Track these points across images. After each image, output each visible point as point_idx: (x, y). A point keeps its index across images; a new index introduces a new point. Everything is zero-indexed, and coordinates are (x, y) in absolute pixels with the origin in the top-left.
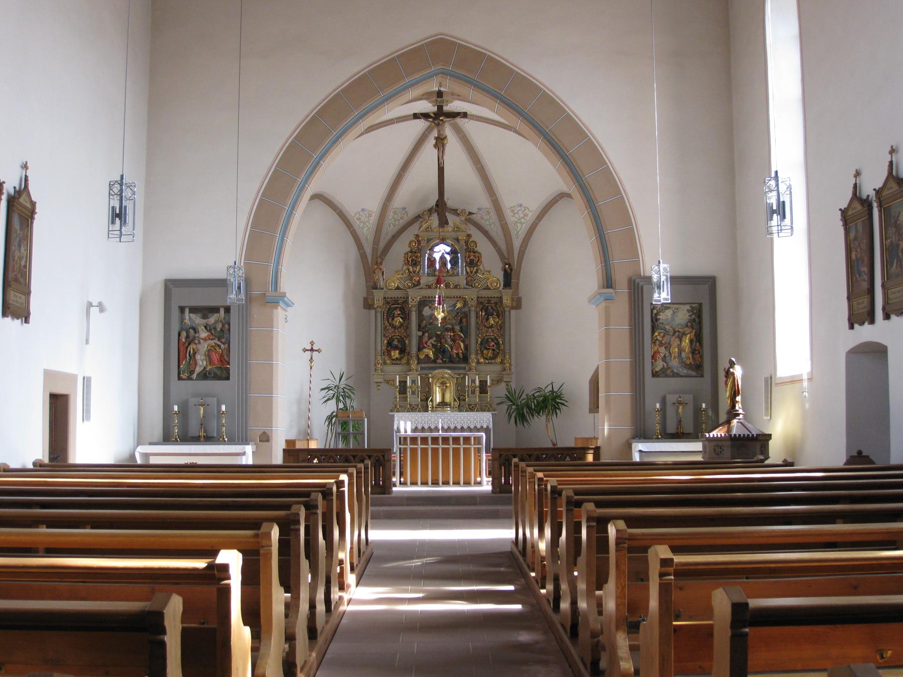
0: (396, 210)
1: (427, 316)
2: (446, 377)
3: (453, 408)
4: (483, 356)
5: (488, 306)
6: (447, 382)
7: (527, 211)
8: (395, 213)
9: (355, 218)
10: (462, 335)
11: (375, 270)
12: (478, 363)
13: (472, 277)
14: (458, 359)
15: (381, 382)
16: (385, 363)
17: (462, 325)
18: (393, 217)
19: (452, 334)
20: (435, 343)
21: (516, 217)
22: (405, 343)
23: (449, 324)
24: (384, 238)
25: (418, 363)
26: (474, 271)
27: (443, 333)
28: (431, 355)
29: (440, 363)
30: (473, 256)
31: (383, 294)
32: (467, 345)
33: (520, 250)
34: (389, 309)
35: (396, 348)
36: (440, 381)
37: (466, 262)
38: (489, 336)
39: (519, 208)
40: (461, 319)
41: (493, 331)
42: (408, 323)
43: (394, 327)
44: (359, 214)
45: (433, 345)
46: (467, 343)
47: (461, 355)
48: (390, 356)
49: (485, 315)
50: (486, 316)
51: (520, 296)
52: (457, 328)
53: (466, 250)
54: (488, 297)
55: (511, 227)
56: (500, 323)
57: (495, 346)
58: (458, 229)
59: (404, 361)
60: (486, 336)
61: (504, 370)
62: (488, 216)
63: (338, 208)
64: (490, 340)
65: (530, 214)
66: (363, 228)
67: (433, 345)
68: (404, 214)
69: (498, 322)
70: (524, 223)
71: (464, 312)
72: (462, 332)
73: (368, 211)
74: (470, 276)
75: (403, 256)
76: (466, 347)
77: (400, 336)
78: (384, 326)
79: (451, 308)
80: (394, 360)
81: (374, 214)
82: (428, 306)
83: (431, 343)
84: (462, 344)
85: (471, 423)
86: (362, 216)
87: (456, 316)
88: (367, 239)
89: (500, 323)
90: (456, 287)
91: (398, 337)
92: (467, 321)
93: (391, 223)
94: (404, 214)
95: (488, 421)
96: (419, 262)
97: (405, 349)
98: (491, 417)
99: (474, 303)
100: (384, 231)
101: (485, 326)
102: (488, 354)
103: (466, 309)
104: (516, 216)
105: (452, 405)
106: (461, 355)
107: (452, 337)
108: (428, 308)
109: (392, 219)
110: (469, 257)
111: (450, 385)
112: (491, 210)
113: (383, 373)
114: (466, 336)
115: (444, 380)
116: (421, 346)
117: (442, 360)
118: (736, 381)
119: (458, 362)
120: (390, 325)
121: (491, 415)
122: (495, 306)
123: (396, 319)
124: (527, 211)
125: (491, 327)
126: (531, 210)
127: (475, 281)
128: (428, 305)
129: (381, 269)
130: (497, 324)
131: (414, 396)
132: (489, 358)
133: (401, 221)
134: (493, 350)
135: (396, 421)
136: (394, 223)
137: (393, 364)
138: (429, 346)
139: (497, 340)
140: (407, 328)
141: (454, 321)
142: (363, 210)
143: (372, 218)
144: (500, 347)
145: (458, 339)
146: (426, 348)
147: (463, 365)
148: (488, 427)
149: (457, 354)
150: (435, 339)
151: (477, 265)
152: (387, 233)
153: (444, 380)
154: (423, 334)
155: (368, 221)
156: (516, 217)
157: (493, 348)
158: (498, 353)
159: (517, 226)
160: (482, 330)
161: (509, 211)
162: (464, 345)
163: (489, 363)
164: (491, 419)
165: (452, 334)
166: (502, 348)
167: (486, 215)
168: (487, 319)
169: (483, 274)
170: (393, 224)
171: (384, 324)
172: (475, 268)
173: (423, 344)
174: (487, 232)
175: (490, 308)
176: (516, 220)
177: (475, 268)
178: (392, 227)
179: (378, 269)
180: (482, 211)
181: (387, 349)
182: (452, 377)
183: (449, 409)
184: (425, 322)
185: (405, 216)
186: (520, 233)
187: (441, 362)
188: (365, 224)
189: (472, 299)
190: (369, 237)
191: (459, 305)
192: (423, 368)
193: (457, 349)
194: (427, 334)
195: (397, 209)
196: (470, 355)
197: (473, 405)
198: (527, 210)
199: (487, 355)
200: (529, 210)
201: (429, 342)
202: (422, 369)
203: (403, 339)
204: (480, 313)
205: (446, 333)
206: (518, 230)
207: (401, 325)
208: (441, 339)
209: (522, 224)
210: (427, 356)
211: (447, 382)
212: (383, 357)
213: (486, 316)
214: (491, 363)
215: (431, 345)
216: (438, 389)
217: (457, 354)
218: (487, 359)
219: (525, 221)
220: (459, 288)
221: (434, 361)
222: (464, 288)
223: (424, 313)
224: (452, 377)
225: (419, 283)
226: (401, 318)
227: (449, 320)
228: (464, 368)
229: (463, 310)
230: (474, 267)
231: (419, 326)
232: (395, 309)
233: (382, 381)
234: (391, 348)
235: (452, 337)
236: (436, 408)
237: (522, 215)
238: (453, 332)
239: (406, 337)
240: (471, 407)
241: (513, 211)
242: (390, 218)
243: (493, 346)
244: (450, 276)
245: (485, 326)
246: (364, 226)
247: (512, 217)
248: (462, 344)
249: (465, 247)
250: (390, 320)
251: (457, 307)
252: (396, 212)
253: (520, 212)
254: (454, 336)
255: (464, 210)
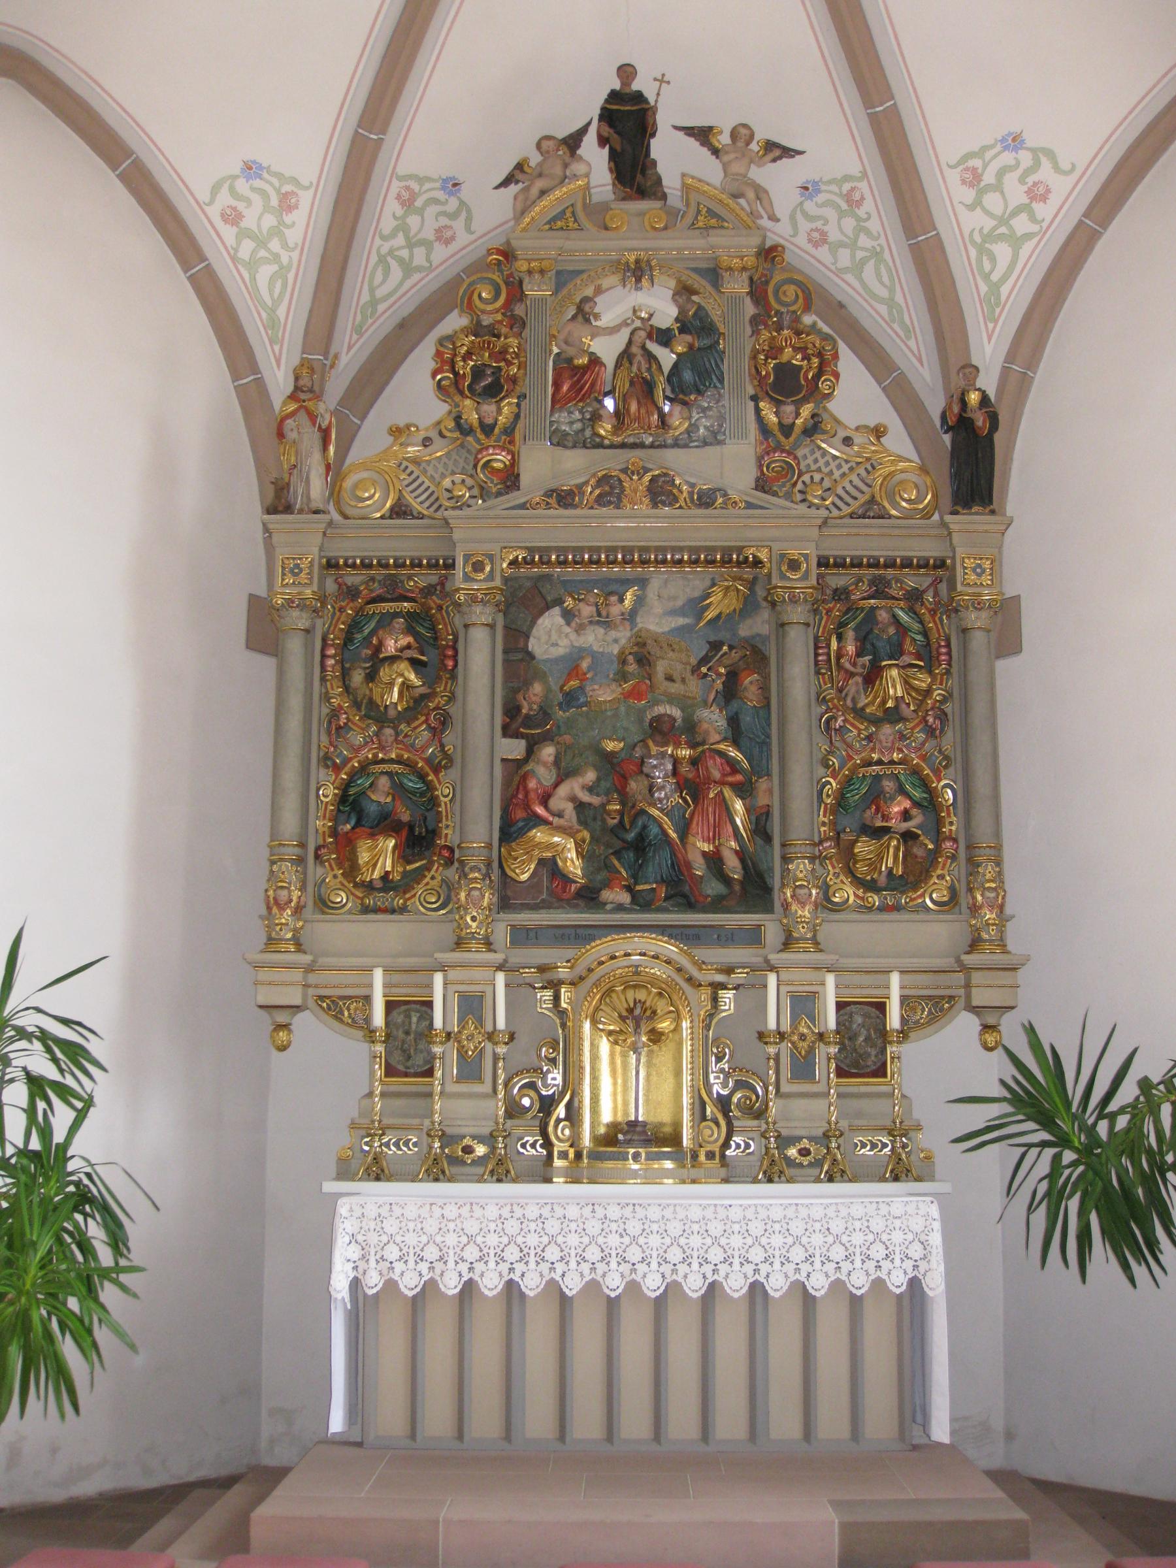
0: (415, 186)
1: (557, 661)
2: (654, 980)
3: (695, 1156)
4: (851, 873)
5: (873, 609)
6: (662, 1006)
7: (1045, 173)
8: (408, 202)
9: (214, 212)
10: (740, 756)
11: (283, 420)
12: (826, 904)
13: (789, 453)
14: (713, 888)
15: (296, 1009)
16: (324, 904)
17: (735, 705)
18: (403, 228)
19: (685, 753)
20: (596, 800)
21: (987, 212)
22: (434, 802)
23: (670, 703)
24: (359, 330)
25: (505, 904)
26: (799, 422)
27: (638, 753)
28: (573, 864)
29: (620, 908)
30: (796, 349)
31: (319, 538)
32: (767, 813)
33: (1005, 372)
34: (354, 626)
35: (385, 823)
36: (620, 1002)
37: (761, 380)
38: (880, 762)
39: (1008, 158)
40: (732, 678)
41: (902, 737)
42: (452, 698)
43: (375, 713)
44: (232, 190)
45: (580, 806)
46: (762, 800)
47: (732, 863)
48: (351, 869)
49: (859, 654)
50: (867, 659)
51: (1010, 592)
52: (713, 720)
53: (755, 321)
54: (875, 565)
55: (960, 260)
56: (937, 694)
57: (918, 818)
58: (713, 222)
59: (423, 895)
60: (868, 763)
61: (975, 944)
62: (849, 224)
63: (128, 152)
64: (888, 785)
65: (1060, 186)
66: (253, 265)
67: (580, 806)
68: (454, 216)
69: (928, 692)
70: (1028, 236)
71: (745, 640)
72: (736, 743)
73: (279, 176)
74: (779, 448)
75: (433, 351)
76: (761, 826)
77: (409, 764)
78: (325, 710)
79: (681, 621)
80: (369, 887)
81: (305, 198)
82: (556, 610)
83: (573, 799)
84: (739, 806)
85: (809, 1259)
86: (249, 202)
87: (704, 661)
88: (272, 324)
89: (937, 694)
90: (705, 500)
91: (396, 767)
92: (764, 688)
93: (391, 252)
94: (454, 216)
95: (916, 1251)
96: (514, 380)
97: (434, 833)
98: (937, 1225)
99: (801, 583)
100: (356, 293)
101: (859, 713)
102: (880, 858)
103: (758, 625)
104: (992, 201)
105: (686, 1142)
106: (732, 863)
107: (685, 769)
108: (561, 621)
109: (393, 235)
110: (774, 351)
111: (677, 1029)
112: (863, 185)
113: (307, 959)
114: (760, 769)
115: (641, 995)
116: (520, 814)
117: (629, 889)
118: (992, 1123)
119: (718, 905)
120: (357, 704)
121: (934, 1210)
122: (912, 611)
123: (384, 673)
124: (1045, 173)
125: (893, 715)
126: (1066, 166)
127: (806, 478)
128: (559, 602)
129: (313, 417)
130: (920, 704)
131: (477, 1088)
132: (883, 880)
133: (440, 252)
134: (908, 837)
135: (341, 1241)
136: (405, 253)
137: (366, 910)
138: (560, 815)
139: (924, 784)
140: (445, 721)
141: (694, 687)
142: (251, 169)
143: (298, 217)
144: (939, 822)
145: (716, 775)
146: (546, 822)
147: (748, 919)
148: (915, 1284)
149: (714, 860)
150: (590, 776)
151: (813, 392)
152: (374, 303)
153: (641, 995)
154: (530, 752)
155: (276, 232)
156: (987, 212)
157: (905, 826)
158: (937, 851)
159: (993, 259)
160: (841, 731)
161: (954, 177)
162: (748, 810)
163: (884, 908)
164: (936, 1239)
165: (685, 753)
166: (953, 825)
167: (842, 214)
168: (872, 676)
169: (848, 441)
170: (400, 261)
171: (326, 697)
172: (806, 410)
173: (527, 806)
174: (841, 306)
175: (883, 616)
176: (989, 224)
177: (806, 410)
178: (396, 273)
179: (303, 417)
180: (821, 198)
181: (334, 832)
182: (689, 979)
183: (668, 1164)
184: (537, 688)
185: (459, 225)
186: (1005, 290)
187: (625, 898)
188: (262, 243)
189: (794, 565)
190: (281, 312)
191: (719, 603)
192: (528, 930)
193: (714, 836)
194: (548, 752)
195: (421, 180)
196: (786, 859)
197: (805, 1143)
198: (1046, 163)
199: (874, 866)
200: (1056, 168)
201: (563, 790)
202: (522, 936)
203: (422, 777)
204: (834, 645)
205: (654, 750)
206: (995, 277)
207: (417, 704)
208: (624, 778)
209: (1016, 242)
210: (550, 867)
211: (662, 1006)
212: (315, 872)
213: (867, 659)
214: (896, 908)
215: (569, 808)
216: (604, 1046)
217: (714, 860)
218: (871, 886)
219: (1035, 228)
220: (724, 506)
221: (589, 897)
222: (750, 505)
223: (534, 645)
224: (689, 979)
225: (510, 479)
226: (415, 663)
227: (670, 679)
228: (754, 937)
229: (745, 630)
230: (798, 404)
231: (511, 710)
232: (386, 621)
233: (297, 1001)
234: (358, 824)
235: (685, 769)
236: (595, 1156)
237: (1016, 194)
238: (692, 745)
239: (437, 770)
240: (792, 1152)
241: (974, 179)
242: (388, 224)
243: (906, 815)
244: (676, 444)
245: (859, 713)
246: (262, 253)
247: (971, 207)
248: (739, 806)
249: (750, 309)
250: (357, 677)
251: (710, 614)
252: (413, 196)
253: (1011, 180)
254: (694, 762)
255: (745, 126)
